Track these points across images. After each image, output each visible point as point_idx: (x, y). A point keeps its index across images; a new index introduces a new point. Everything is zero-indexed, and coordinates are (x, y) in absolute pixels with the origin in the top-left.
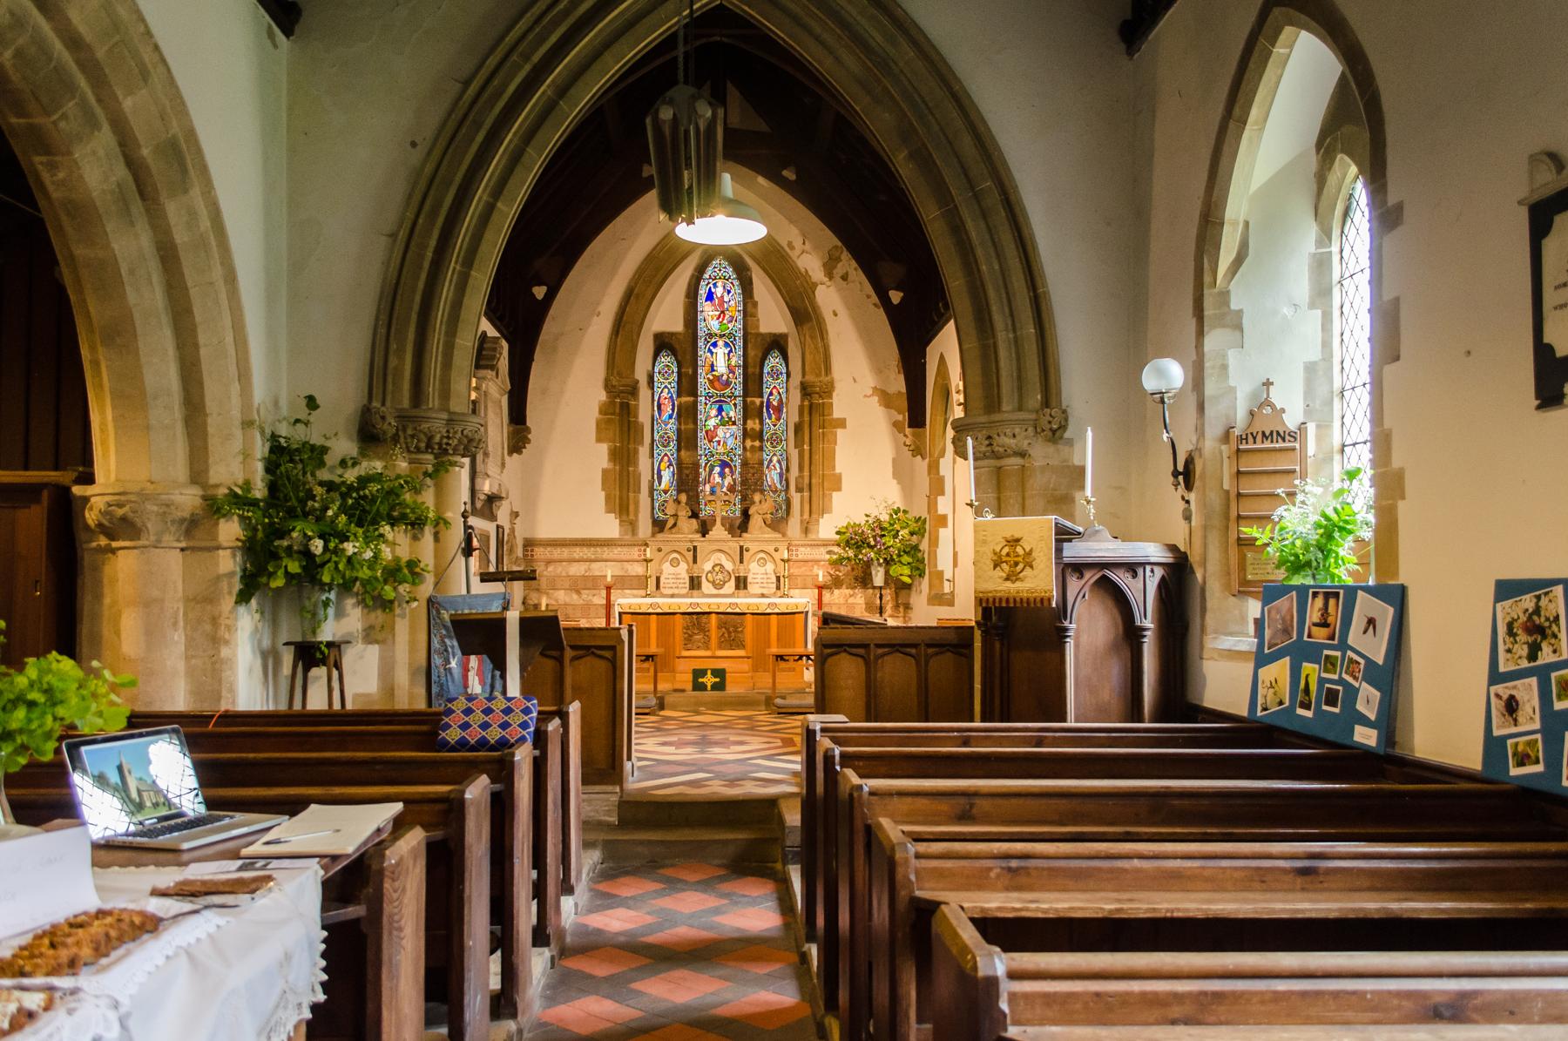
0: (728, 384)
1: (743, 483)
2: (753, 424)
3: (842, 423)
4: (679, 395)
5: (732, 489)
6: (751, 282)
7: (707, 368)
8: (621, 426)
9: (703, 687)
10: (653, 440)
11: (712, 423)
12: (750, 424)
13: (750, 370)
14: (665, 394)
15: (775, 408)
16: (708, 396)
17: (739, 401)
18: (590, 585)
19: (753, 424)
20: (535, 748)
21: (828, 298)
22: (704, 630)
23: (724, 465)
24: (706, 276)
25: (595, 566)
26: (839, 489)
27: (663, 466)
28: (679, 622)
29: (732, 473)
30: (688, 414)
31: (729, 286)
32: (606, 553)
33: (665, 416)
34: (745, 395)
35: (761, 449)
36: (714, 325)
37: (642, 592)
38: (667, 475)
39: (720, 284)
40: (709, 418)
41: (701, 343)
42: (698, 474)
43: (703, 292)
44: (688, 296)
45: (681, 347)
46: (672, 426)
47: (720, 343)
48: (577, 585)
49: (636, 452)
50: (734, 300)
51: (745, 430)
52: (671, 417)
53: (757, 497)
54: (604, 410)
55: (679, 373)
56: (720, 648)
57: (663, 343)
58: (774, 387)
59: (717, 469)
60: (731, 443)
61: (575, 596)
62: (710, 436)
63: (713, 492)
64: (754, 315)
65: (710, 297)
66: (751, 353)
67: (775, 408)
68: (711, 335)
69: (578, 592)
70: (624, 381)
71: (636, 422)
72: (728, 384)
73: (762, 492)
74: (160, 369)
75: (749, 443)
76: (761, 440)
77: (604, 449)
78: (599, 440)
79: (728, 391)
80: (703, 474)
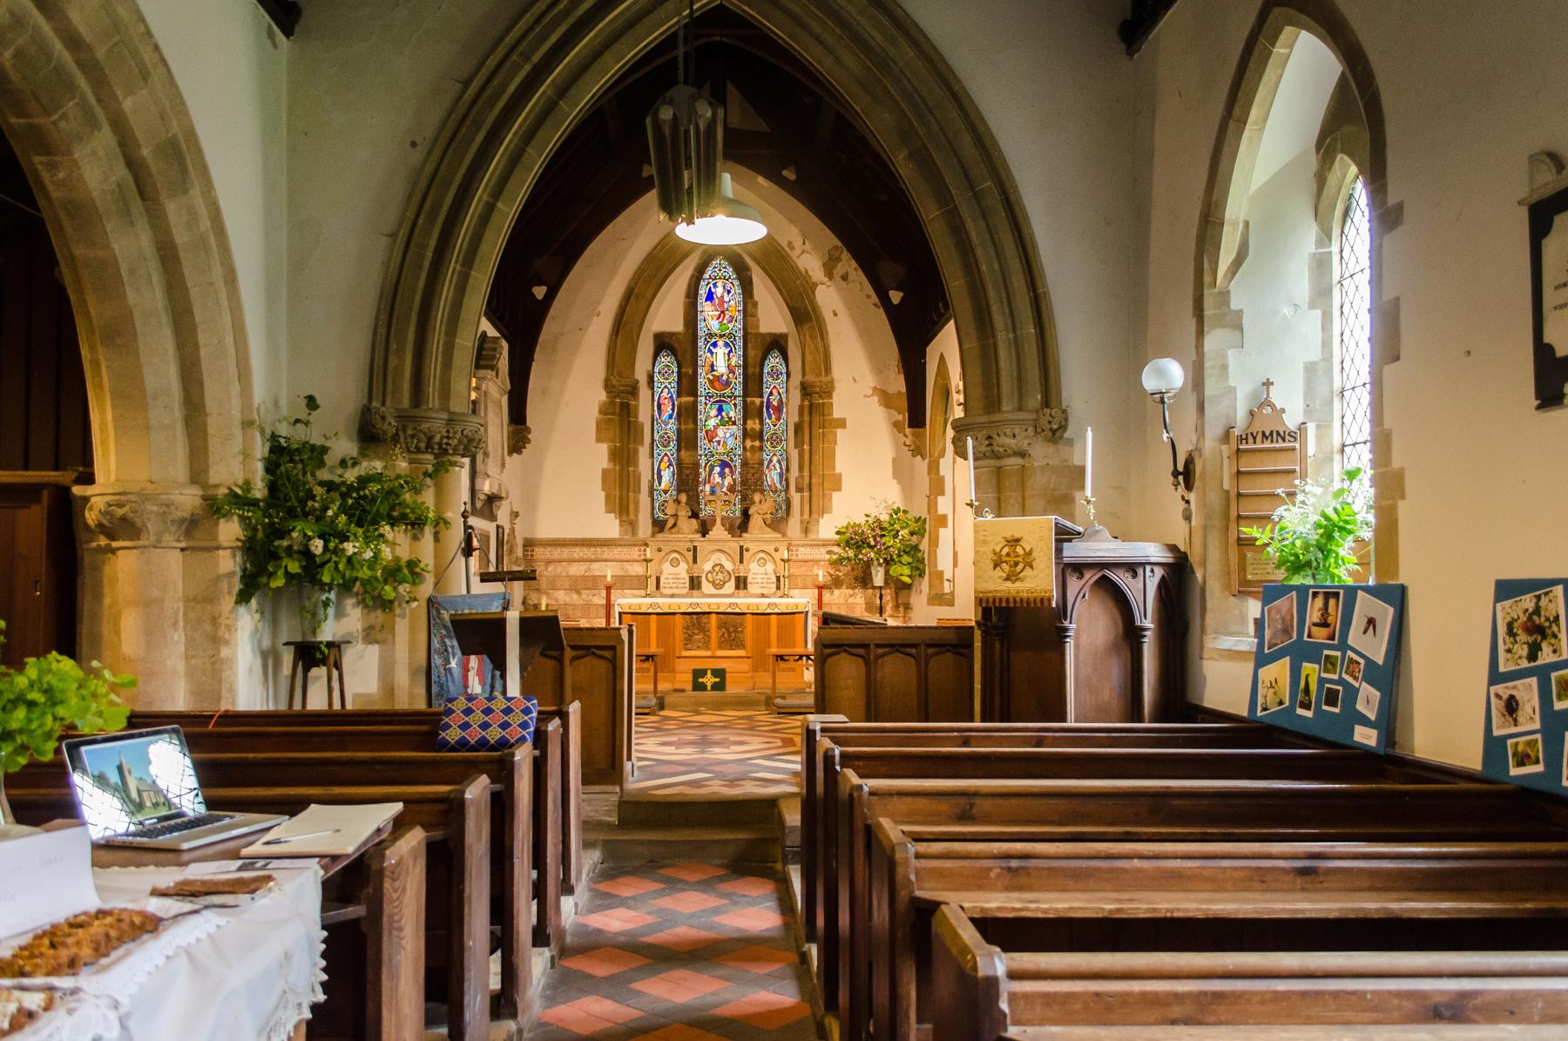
0: (728, 384)
1: (743, 483)
2: (753, 424)
3: (842, 423)
5: (732, 489)
6: (751, 282)
7: (707, 368)
9: (702, 687)
10: (653, 440)
11: (712, 423)
12: (750, 424)
13: (750, 370)
14: (665, 394)
15: (774, 408)
16: (708, 396)
17: (739, 400)
19: (753, 424)
20: (535, 748)
21: (828, 298)
22: (704, 630)
23: (724, 465)
24: (706, 276)
25: (595, 566)
26: (839, 489)
27: (663, 466)
29: (732, 473)
30: (688, 414)
31: (729, 286)
32: (606, 553)
33: (665, 416)
34: (745, 395)
35: (761, 449)
36: (714, 325)
37: (642, 592)
38: (667, 475)
39: (720, 284)
40: (709, 418)
41: (701, 343)
42: (698, 474)
43: (703, 292)
44: (688, 296)
45: (681, 347)
46: (672, 426)
47: (720, 343)
48: (577, 585)
49: (636, 452)
50: (734, 300)
51: (745, 430)
52: (671, 417)
53: (757, 497)
54: (605, 410)
55: (679, 373)
56: (720, 648)
57: (663, 343)
58: (774, 387)
59: (717, 469)
61: (575, 596)
62: (710, 436)
63: (713, 492)
64: (754, 315)
65: (710, 297)
66: (751, 353)
67: (774, 408)
68: (711, 335)
69: (578, 592)
70: (624, 381)
71: (636, 422)
72: (728, 384)
73: (762, 492)
75: (749, 443)
76: (761, 440)
77: (604, 448)
78: (599, 440)
79: (728, 391)
80: (703, 474)
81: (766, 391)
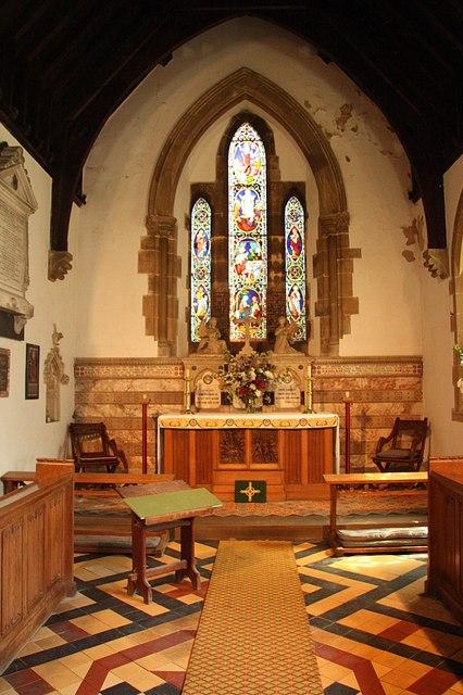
0: (254, 225)
3: (357, 253)
4: (212, 235)
5: (258, 314)
6: (272, 141)
7: (236, 212)
8: (161, 256)
9: (256, 485)
10: (190, 274)
11: (240, 259)
12: (274, 258)
14: (200, 235)
15: (294, 245)
17: (264, 239)
18: (132, 399)
21: (340, 145)
22: (239, 445)
23: (252, 294)
25: (137, 383)
26: (357, 312)
28: (216, 439)
30: (220, 251)
32: (146, 371)
33: (201, 254)
36: (243, 179)
37: (179, 407)
40: (236, 252)
41: (231, 192)
42: (228, 303)
44: (220, 153)
45: (215, 194)
46: (207, 262)
48: (121, 400)
49: (174, 282)
50: (259, 154)
51: (269, 264)
52: (205, 254)
54: (145, 244)
56: (254, 461)
57: (198, 192)
58: (294, 226)
59: (246, 298)
60: (257, 275)
61: (119, 410)
62: (240, 270)
64: (276, 168)
65: (238, 153)
66: (274, 199)
67: (294, 245)
68: (239, 186)
69: (122, 407)
70: (162, 219)
71: (174, 256)
72: (254, 225)
74: (397, 506)
75: (273, 275)
76: (284, 272)
77: (145, 278)
78: (141, 271)
79: (254, 232)
80: (233, 302)
81: (287, 231)
